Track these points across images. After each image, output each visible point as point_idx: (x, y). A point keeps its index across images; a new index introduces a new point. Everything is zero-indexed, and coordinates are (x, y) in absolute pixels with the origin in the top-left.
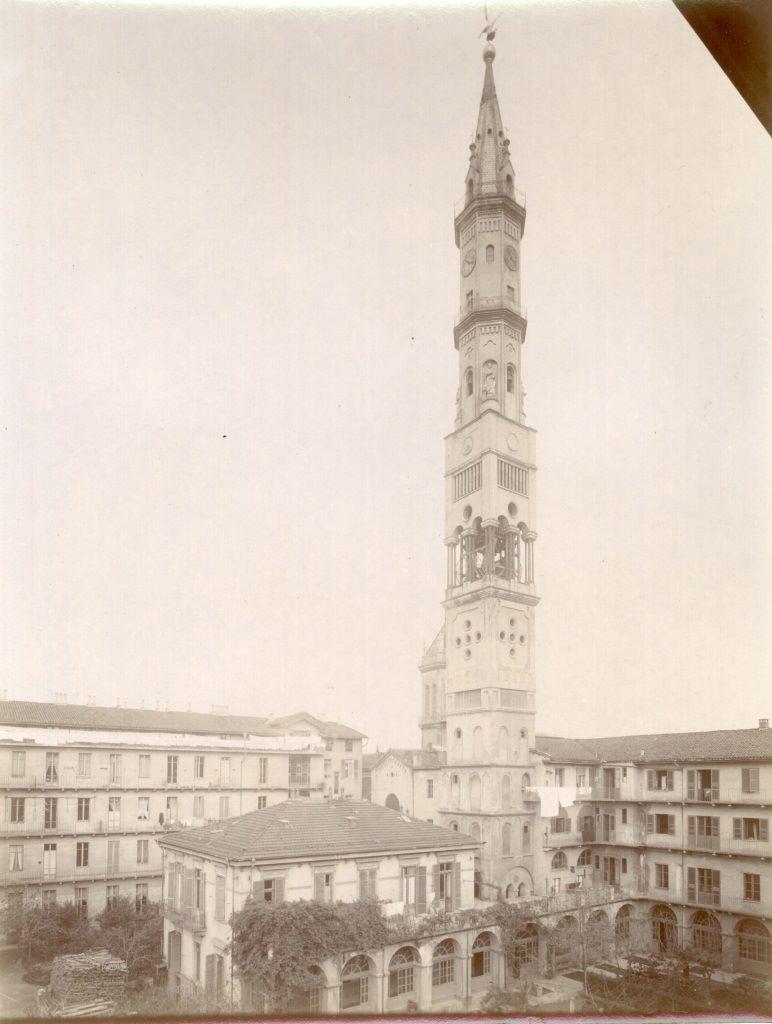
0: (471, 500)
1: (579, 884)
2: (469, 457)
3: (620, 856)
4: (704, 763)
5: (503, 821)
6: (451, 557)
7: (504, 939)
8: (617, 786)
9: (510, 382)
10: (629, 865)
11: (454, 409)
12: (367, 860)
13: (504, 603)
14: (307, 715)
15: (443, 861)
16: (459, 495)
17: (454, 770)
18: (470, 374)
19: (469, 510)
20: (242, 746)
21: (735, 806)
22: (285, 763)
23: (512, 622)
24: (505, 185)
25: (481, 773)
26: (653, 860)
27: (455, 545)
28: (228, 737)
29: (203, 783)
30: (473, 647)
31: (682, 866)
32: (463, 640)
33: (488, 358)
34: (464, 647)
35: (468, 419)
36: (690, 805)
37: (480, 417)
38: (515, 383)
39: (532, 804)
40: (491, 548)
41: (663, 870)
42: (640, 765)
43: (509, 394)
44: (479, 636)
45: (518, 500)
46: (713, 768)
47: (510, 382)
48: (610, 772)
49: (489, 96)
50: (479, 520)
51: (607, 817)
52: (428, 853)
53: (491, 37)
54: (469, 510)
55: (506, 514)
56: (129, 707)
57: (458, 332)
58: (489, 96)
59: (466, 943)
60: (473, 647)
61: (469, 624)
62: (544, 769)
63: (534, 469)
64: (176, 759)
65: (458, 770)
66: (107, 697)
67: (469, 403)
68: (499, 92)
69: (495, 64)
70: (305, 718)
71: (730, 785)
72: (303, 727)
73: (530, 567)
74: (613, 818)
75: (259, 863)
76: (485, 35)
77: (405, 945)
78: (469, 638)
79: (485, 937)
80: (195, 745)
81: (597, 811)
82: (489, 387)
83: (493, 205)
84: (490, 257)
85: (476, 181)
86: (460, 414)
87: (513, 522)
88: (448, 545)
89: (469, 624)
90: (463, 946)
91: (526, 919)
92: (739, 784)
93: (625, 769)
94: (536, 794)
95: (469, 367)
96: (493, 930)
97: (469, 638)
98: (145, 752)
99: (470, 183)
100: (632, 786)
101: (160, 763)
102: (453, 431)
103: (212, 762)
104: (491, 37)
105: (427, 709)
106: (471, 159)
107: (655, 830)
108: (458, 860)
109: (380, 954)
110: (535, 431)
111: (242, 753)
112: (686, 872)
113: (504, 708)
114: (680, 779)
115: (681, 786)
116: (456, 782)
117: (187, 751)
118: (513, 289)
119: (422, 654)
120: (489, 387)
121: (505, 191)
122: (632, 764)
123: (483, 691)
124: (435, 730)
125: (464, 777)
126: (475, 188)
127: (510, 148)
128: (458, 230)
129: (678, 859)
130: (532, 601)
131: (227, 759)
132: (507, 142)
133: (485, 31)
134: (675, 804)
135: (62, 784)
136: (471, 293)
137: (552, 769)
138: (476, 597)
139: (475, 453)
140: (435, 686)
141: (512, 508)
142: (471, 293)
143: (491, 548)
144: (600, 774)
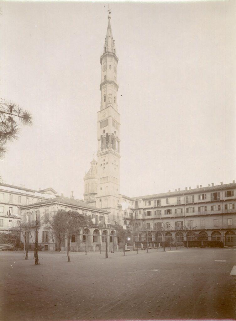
0: (106, 128)
2: (104, 118)
3: (138, 222)
4: (157, 198)
6: (99, 143)
7: (117, 233)
8: (138, 205)
9: (115, 101)
10: (141, 224)
11: (100, 105)
14: (52, 189)
15: (101, 215)
16: (101, 127)
17: (100, 198)
18: (105, 97)
19: (104, 131)
21: (165, 207)
23: (115, 161)
24: (114, 51)
25: (108, 197)
26: (147, 222)
27: (100, 140)
30: (105, 166)
31: (153, 223)
32: (103, 164)
33: (110, 93)
34: (103, 166)
35: (104, 108)
36: (155, 208)
37: (108, 107)
38: (116, 101)
39: (120, 207)
40: (108, 141)
41: (149, 224)
42: (144, 200)
43: (114, 104)
44: (107, 163)
45: (116, 131)
46: (160, 199)
47: (115, 101)
48: (136, 202)
49: (109, 27)
50: (107, 134)
51: (136, 213)
53: (110, 13)
54: (104, 131)
55: (114, 133)
57: (101, 86)
58: (109, 27)
59: (109, 232)
60: (105, 166)
61: (104, 160)
62: (122, 198)
63: (120, 124)
65: (101, 198)
67: (104, 104)
68: (111, 27)
69: (111, 20)
70: (51, 190)
71: (163, 203)
72: (50, 192)
73: (119, 148)
74: (137, 213)
75: (60, 203)
76: (108, 12)
77: (97, 229)
78: (104, 164)
79: (112, 232)
81: (133, 212)
82: (107, 102)
83: (109, 55)
84: (110, 68)
85: (106, 48)
86: (101, 107)
87: (115, 136)
88: (98, 140)
89: (104, 160)
90: (108, 232)
92: (165, 202)
93: (140, 201)
94: (121, 204)
95: (105, 95)
96: (115, 231)
97: (104, 164)
99: (105, 48)
100: (142, 205)
102: (100, 111)
104: (110, 13)
105: (86, 190)
106: (105, 42)
107: (147, 215)
108: (104, 216)
109: (91, 229)
110: (120, 115)
111: (33, 197)
112: (154, 224)
114: (152, 202)
115: (153, 203)
116: (100, 201)
118: (115, 78)
119: (85, 175)
120: (107, 102)
121: (114, 52)
124: (89, 196)
125: (103, 199)
126: (106, 49)
127: (115, 42)
128: (101, 59)
129: (152, 221)
130: (119, 157)
131: (28, 198)
132: (114, 41)
133: (108, 11)
134: (152, 208)
136: (105, 76)
138: (106, 153)
139: (106, 116)
140: (89, 184)
142: (105, 76)
143: (108, 141)
144: (134, 202)
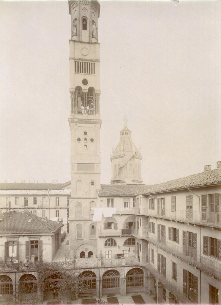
1: (124, 254)
5: (76, 223)
12: (12, 237)
13: (79, 125)
20: (47, 193)
22: (65, 199)
28: (45, 190)
29: (36, 206)
43: (83, 31)
52: (24, 236)
56: (25, 183)
64: (59, 198)
66: (49, 180)
80: (31, 194)
91: (52, 271)
98: (16, 196)
101: (54, 199)
103: (39, 199)
113: (79, 172)
117: (39, 196)
122: (141, 196)
123: (95, 165)
135: (61, 206)
137: (105, 200)
141: (85, 82)
